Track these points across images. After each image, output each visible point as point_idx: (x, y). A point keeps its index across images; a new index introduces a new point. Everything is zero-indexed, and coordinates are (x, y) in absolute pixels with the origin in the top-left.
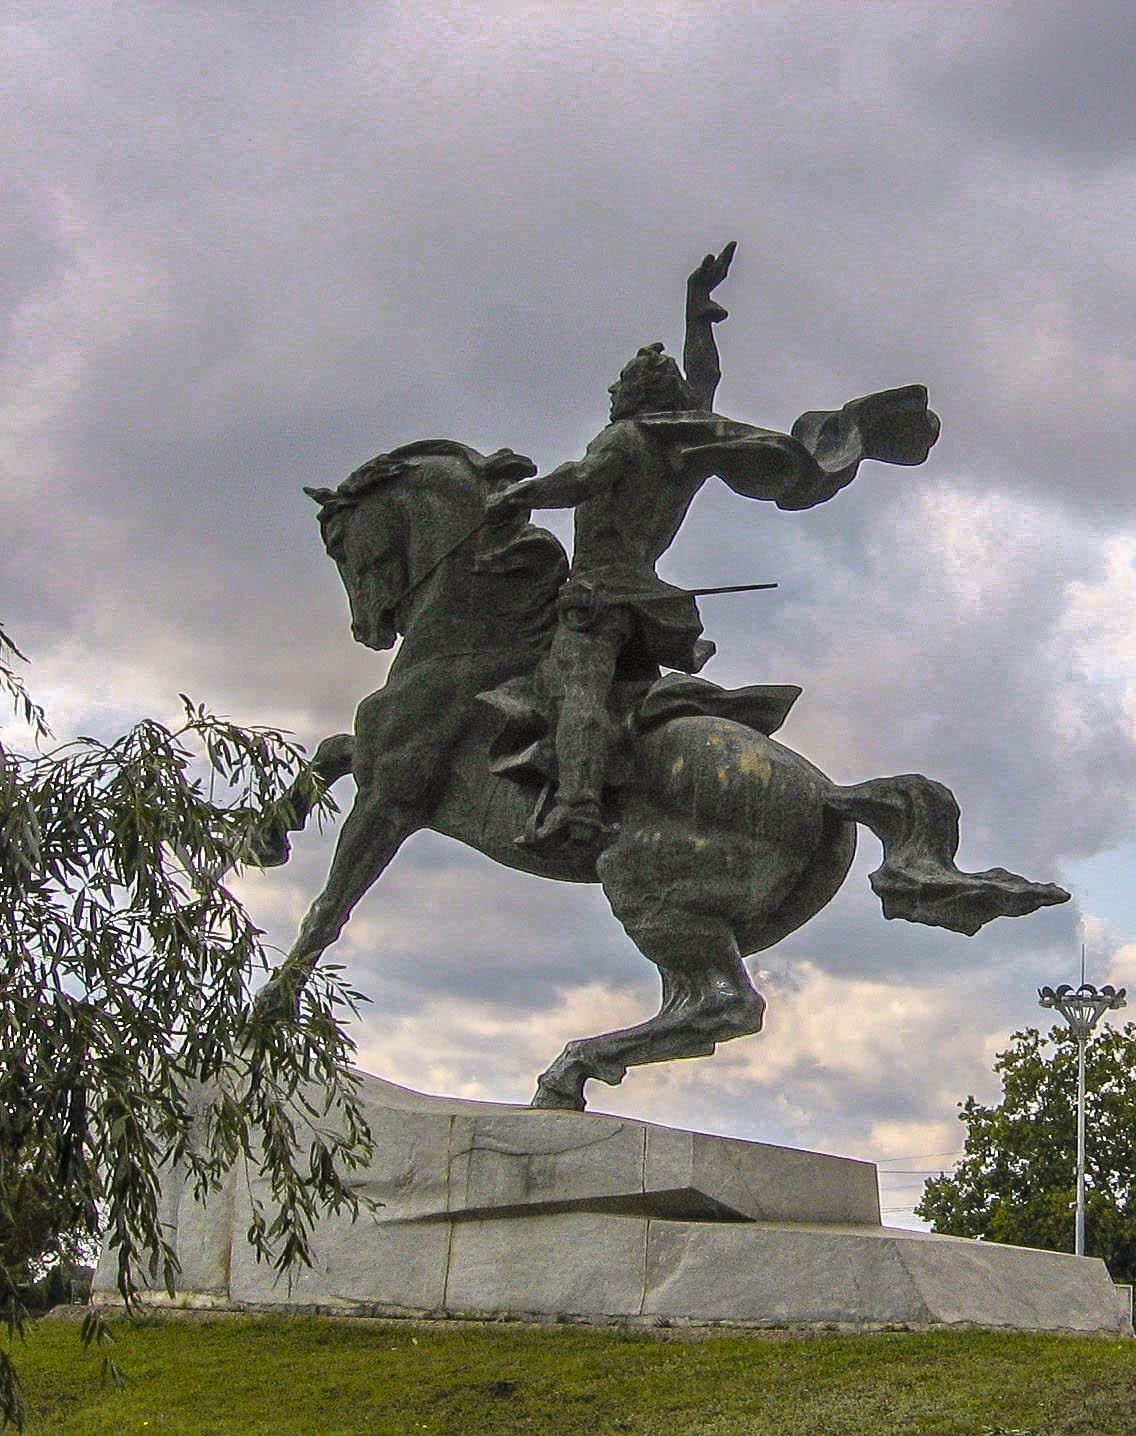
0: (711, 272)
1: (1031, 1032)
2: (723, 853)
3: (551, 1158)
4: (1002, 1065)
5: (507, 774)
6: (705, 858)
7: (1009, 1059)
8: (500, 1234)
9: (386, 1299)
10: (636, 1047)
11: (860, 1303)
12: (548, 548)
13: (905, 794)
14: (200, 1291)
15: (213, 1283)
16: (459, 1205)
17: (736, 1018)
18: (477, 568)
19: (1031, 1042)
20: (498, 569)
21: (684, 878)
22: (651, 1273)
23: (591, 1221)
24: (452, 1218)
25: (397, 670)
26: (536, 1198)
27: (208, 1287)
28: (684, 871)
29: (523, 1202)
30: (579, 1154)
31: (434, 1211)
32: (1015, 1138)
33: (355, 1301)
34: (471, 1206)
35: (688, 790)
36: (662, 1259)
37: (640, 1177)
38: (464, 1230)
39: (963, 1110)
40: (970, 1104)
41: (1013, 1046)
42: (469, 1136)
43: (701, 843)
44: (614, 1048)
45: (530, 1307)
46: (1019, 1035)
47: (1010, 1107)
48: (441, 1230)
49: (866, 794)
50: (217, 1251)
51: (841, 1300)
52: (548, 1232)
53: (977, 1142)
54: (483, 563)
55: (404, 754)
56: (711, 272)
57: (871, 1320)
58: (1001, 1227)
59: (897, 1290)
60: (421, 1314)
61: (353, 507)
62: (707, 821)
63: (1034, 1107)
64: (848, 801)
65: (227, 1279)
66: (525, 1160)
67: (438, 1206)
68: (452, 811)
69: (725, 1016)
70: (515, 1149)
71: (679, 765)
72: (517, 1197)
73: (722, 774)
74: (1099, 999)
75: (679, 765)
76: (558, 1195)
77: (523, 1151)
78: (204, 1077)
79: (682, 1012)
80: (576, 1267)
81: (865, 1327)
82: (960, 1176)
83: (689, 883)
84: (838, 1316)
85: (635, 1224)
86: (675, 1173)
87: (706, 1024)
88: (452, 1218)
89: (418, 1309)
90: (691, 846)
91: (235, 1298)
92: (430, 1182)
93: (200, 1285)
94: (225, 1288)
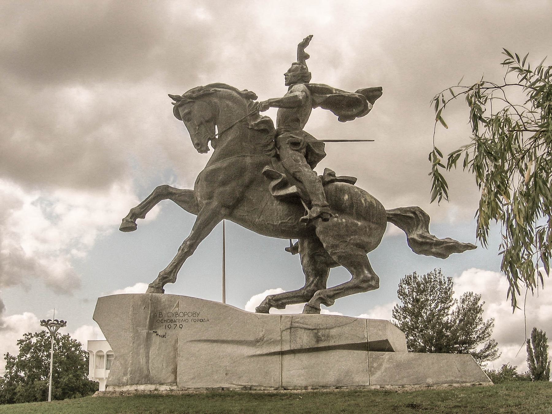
0: (307, 41)
1: (30, 334)
2: (366, 227)
3: (327, 330)
4: (19, 343)
5: (278, 198)
6: (361, 229)
7: (21, 342)
8: (305, 359)
9: (254, 384)
10: (337, 293)
11: (461, 377)
12: (268, 122)
13: (414, 213)
14: (162, 384)
15: (170, 381)
16: (286, 348)
17: (373, 283)
18: (250, 127)
19: (29, 337)
20: (256, 128)
21: (355, 235)
22: (371, 371)
23: (345, 352)
24: (282, 353)
25: (212, 161)
26: (322, 345)
27: (167, 382)
28: (355, 232)
29: (316, 346)
30: (340, 328)
31: (275, 351)
32: (22, 365)
33: (241, 385)
34: (292, 348)
35: (352, 206)
36: (375, 365)
37: (366, 336)
38: (287, 358)
39: (5, 356)
40: (8, 355)
41: (23, 338)
42: (290, 323)
43: (359, 223)
44: (332, 293)
45: (321, 384)
46: (26, 334)
47: (20, 356)
48: (277, 358)
49: (399, 212)
50: (170, 368)
51: (453, 376)
52: (323, 357)
53: (10, 365)
54: (252, 125)
55: (228, 188)
56: (307, 41)
57: (465, 382)
58: (19, 392)
59: (475, 372)
60: (273, 389)
61: (194, 102)
62: (359, 216)
63: (28, 356)
64: (392, 214)
65: (176, 379)
66: (316, 331)
67: (278, 349)
68: (241, 212)
69: (370, 283)
70: (311, 327)
71: (346, 197)
72: (313, 344)
73: (363, 201)
74: (59, 324)
75: (346, 197)
76: (332, 343)
77: (314, 328)
78: (425, 276)
79: (356, 282)
80: (295, 373)
81: (464, 384)
82: (6, 376)
83: (356, 237)
84: (452, 382)
85: (363, 354)
86: (373, 337)
87: (364, 285)
88: (282, 353)
89: (271, 387)
90: (358, 224)
91: (180, 386)
92: (272, 340)
93: (162, 382)
94: (175, 382)
